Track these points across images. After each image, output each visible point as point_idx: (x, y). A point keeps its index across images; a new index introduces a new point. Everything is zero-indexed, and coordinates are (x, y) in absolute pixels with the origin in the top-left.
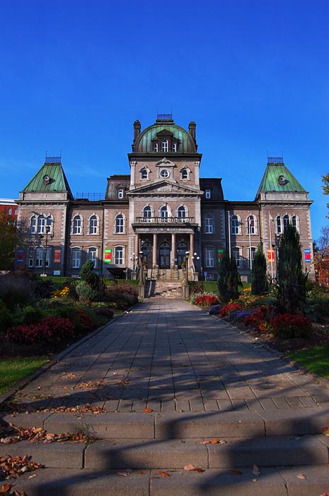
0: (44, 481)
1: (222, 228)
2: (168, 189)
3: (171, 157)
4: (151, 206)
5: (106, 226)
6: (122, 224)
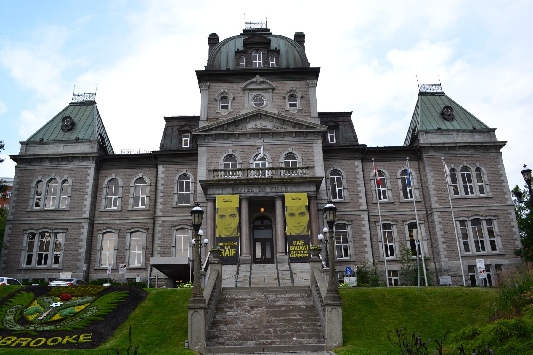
0: (284, 82)
1: (360, 192)
2: (267, 125)
3: (267, 73)
4: (237, 154)
5: (160, 194)
6: (188, 189)
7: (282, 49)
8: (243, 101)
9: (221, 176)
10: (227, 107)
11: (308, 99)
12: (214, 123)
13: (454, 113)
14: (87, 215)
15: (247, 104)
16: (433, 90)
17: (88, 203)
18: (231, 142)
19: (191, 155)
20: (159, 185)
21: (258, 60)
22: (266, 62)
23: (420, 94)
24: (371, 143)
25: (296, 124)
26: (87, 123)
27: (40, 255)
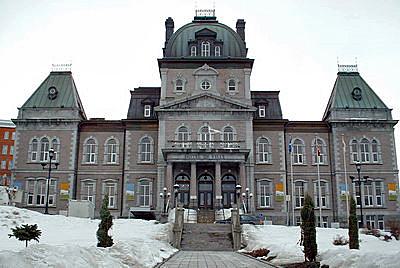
2: (211, 104)
3: (214, 63)
5: (128, 153)
7: (226, 41)
8: (197, 82)
9: (222, 146)
10: (181, 89)
11: (244, 83)
12: (171, 103)
13: (363, 94)
14: (73, 168)
15: (197, 88)
16: (350, 70)
17: (73, 158)
18: (183, 117)
19: (154, 121)
20: (127, 146)
21: (206, 50)
22: (212, 52)
23: (339, 73)
24: (291, 119)
25: (233, 105)
26: (68, 93)
27: (39, 197)
